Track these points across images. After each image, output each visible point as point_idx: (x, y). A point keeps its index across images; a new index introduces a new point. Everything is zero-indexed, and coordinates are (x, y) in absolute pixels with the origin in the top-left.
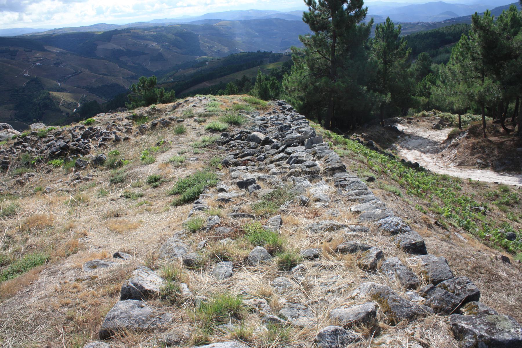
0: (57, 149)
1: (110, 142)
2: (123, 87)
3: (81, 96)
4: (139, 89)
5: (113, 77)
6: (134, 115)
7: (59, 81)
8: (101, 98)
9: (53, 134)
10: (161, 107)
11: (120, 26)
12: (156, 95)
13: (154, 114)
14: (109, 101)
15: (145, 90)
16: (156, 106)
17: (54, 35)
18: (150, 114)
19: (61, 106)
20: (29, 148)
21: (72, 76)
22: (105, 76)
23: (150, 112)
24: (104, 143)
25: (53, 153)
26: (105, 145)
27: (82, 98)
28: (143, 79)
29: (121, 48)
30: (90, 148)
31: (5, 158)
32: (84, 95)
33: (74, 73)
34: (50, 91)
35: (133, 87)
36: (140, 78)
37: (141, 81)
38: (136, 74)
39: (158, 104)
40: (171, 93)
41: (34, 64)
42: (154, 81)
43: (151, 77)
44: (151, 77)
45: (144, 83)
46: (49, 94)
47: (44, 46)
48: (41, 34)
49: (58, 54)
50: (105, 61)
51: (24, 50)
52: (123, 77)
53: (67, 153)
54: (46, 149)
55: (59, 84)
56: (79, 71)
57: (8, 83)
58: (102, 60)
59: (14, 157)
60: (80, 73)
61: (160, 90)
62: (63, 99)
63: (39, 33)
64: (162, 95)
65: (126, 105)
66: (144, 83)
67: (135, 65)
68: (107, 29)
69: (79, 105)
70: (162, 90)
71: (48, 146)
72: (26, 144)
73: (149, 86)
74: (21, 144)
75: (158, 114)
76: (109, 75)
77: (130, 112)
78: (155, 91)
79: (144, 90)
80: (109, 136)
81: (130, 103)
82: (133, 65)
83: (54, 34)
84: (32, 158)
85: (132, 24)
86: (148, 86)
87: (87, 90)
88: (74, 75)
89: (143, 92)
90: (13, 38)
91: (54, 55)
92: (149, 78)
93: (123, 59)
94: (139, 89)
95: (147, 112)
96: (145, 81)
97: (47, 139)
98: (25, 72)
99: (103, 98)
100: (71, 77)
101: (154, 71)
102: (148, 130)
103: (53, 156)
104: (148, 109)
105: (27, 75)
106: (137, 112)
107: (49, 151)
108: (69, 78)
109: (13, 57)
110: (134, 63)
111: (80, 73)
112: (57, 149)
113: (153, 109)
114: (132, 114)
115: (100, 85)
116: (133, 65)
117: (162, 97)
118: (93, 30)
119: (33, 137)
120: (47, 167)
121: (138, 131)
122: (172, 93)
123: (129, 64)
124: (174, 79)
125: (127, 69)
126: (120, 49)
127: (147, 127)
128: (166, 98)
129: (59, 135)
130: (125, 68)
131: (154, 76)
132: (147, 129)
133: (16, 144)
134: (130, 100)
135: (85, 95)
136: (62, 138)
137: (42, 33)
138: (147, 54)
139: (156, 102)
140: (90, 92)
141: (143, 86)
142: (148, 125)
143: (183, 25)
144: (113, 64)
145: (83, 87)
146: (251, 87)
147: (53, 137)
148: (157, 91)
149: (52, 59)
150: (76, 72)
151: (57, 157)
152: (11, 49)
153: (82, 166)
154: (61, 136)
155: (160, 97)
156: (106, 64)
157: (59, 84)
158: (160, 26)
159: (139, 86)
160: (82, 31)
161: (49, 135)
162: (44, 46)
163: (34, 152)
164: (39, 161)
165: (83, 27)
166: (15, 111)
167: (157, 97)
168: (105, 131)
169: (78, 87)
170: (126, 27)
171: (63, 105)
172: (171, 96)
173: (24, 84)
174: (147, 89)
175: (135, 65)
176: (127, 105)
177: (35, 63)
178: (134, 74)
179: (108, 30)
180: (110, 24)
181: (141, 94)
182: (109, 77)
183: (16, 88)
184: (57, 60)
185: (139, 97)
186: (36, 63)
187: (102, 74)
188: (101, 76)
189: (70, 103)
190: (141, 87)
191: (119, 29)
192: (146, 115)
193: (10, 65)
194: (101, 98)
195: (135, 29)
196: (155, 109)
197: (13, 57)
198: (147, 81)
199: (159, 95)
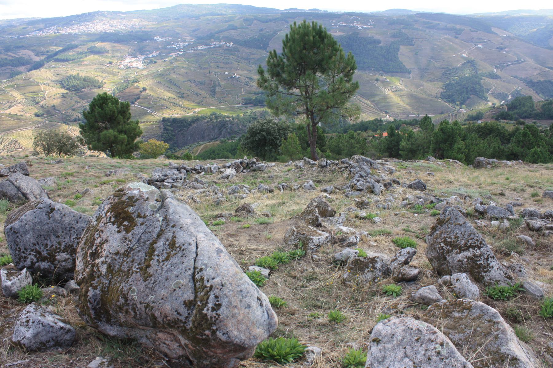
3: (515, 88)
7: (496, 67)
17: (506, 17)
27: (516, 90)
69: (510, 97)
83: (507, 15)
98: (464, 53)
99: (541, 95)
115: (542, 80)
135: (520, 88)
150: (517, 61)
157: (495, 70)
166: (442, 90)
173: (459, 65)
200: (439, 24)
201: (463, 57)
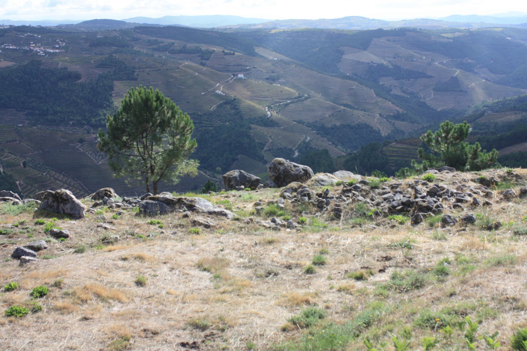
0: (398, 204)
1: (466, 205)
2: (378, 132)
4: (437, 141)
5: (362, 113)
6: (482, 178)
8: (336, 146)
9: (389, 187)
10: (521, 172)
11: (386, 23)
12: (466, 155)
13: (511, 180)
14: (350, 154)
15: (448, 144)
16: (513, 169)
17: (273, 31)
18: (504, 179)
19: (266, 150)
20: (360, 198)
21: (293, 103)
22: (348, 109)
23: (504, 177)
24: (459, 204)
25: (394, 207)
26: (460, 207)
27: (304, 142)
28: (447, 126)
29: (385, 63)
30: (443, 207)
31: (336, 205)
32: (306, 138)
33: (295, 98)
34: (252, 124)
35: (428, 136)
36: (443, 124)
37: (443, 129)
38: (405, 112)
39: (468, 170)
40: (490, 153)
41: (234, 75)
42: (465, 131)
43: (462, 124)
44: (462, 124)
45: (447, 132)
46: (250, 128)
47: (255, 48)
48: (252, 27)
49: (274, 63)
50: (352, 82)
51: (223, 52)
52: (380, 115)
53: (410, 210)
54: (382, 202)
55: (269, 113)
56: (306, 95)
57: (188, 102)
58: (348, 81)
59: (345, 206)
60: (306, 98)
61: (474, 146)
62: (271, 141)
63: (250, 25)
64: (475, 155)
65: (412, 164)
66: (447, 132)
67: (405, 95)
68: (364, 27)
70: (477, 148)
71: (385, 199)
72: (357, 193)
73: (456, 139)
74: (351, 192)
75: (517, 181)
76: (356, 107)
77: (476, 174)
78: (463, 148)
79: (446, 143)
80: (463, 197)
81: (420, 163)
82: (402, 94)
84: (368, 210)
85: (410, 21)
86: (454, 138)
87: (313, 130)
88: (297, 102)
89: (443, 147)
90: (209, 31)
91: (269, 64)
92: (457, 126)
93: (385, 81)
94: (437, 141)
95: (500, 177)
96: (450, 130)
97: (380, 191)
99: (339, 147)
100: (290, 103)
101: (439, 110)
102: (516, 197)
103: (393, 211)
104: (19, 187)
105: (220, 92)
106: (486, 174)
107: (386, 205)
108: (286, 105)
109: (204, 61)
110: (404, 92)
111: (306, 98)
112: (398, 204)
113: (509, 173)
114: (479, 177)
115: (338, 124)
116: (402, 94)
117: (475, 159)
118: (340, 26)
119: (362, 186)
120: (389, 221)
121: (502, 196)
122: (493, 154)
123: (395, 92)
124: (474, 128)
125: (390, 101)
126: (382, 65)
127: (514, 194)
128: (482, 161)
129: (397, 187)
130: (386, 99)
131: (465, 123)
132: (514, 196)
133: (344, 192)
134: (421, 156)
135: (308, 138)
136: (401, 193)
137: (255, 25)
138: (430, 77)
139: (464, 165)
140: (318, 134)
141: (446, 137)
142: (516, 190)
143: (507, 30)
144: (365, 88)
145: (309, 123)
146: (440, 163)
147: (388, 189)
148: (468, 149)
149: (264, 71)
150: (299, 97)
151: (399, 212)
152: (204, 47)
153: (451, 223)
154: (398, 189)
155: (471, 158)
156: (354, 87)
158: (461, 28)
159: (439, 135)
160: (321, 27)
161: (384, 187)
162: (255, 48)
163: (369, 203)
164: (377, 214)
165: (323, 21)
167: (467, 159)
168: (455, 191)
169: (300, 122)
170: (398, 26)
171: (269, 150)
172: (491, 160)
173: (213, 108)
174: (452, 142)
175: (405, 95)
176: (414, 163)
177: (235, 73)
178: (401, 111)
179: (366, 29)
180: (371, 18)
181: (439, 149)
182: (356, 112)
183: (199, 113)
184: (273, 72)
185: (436, 154)
186: (237, 75)
187: (345, 105)
188: (342, 107)
189: (281, 149)
190: (442, 138)
191: (386, 28)
192: (499, 180)
193: (197, 74)
194: (336, 146)
195: (414, 30)
196: (512, 174)
197: (204, 61)
198: (453, 130)
199: (470, 156)
200: (173, 43)
201: (218, 96)
